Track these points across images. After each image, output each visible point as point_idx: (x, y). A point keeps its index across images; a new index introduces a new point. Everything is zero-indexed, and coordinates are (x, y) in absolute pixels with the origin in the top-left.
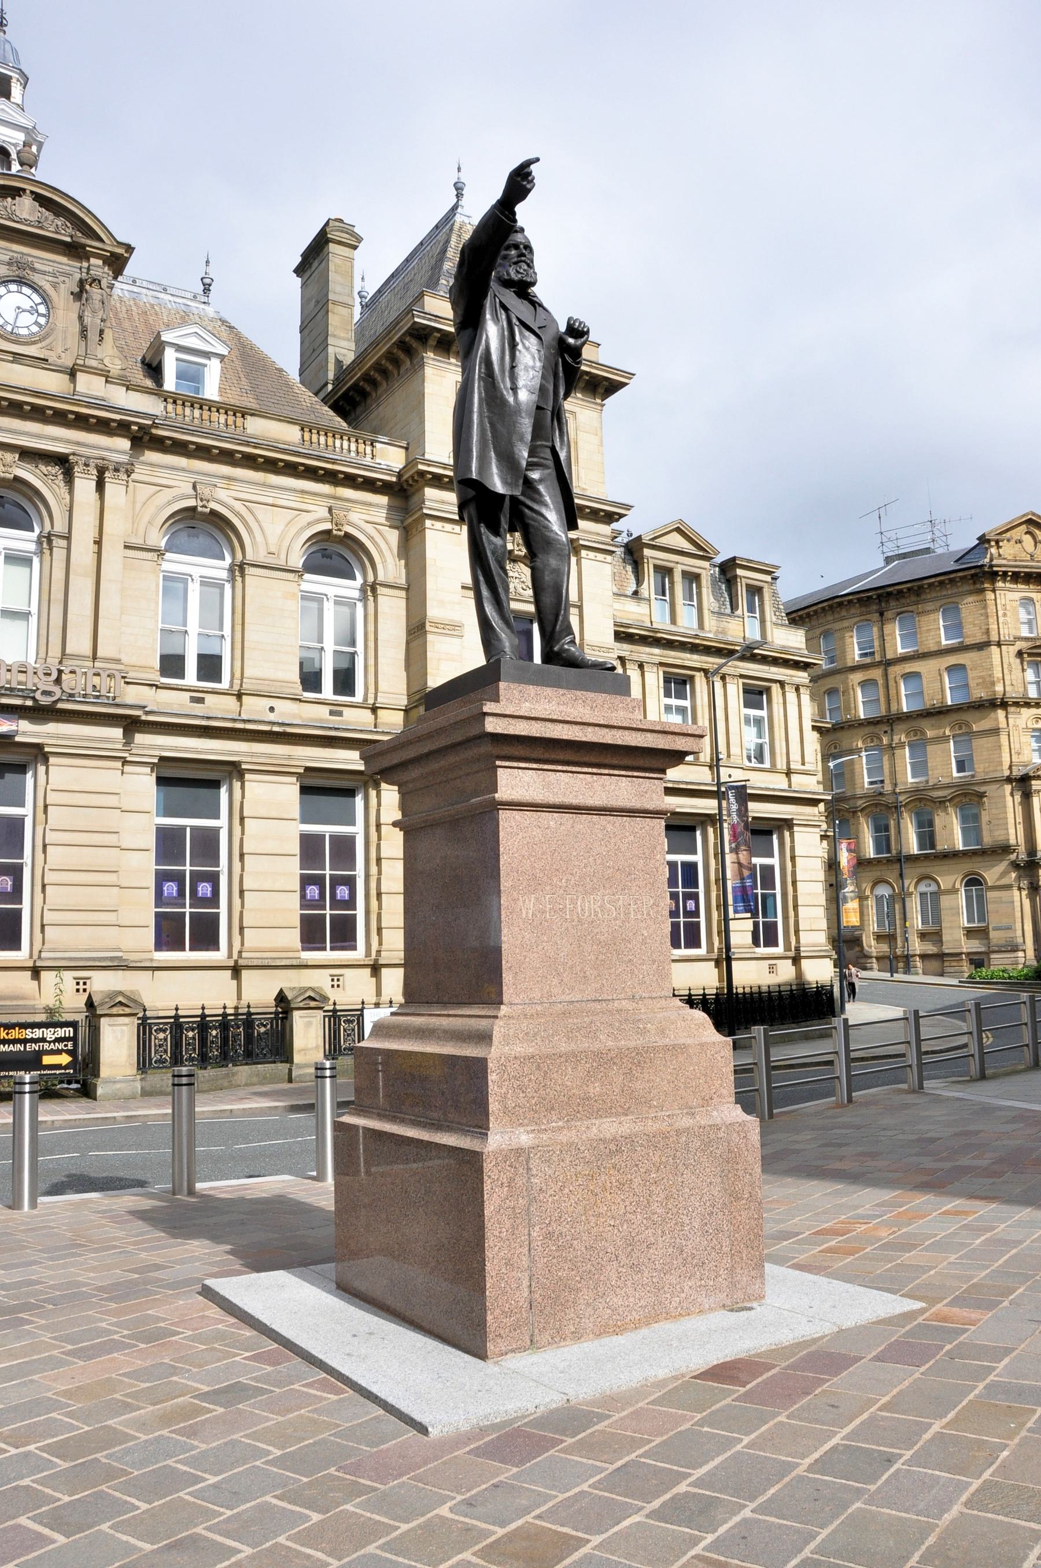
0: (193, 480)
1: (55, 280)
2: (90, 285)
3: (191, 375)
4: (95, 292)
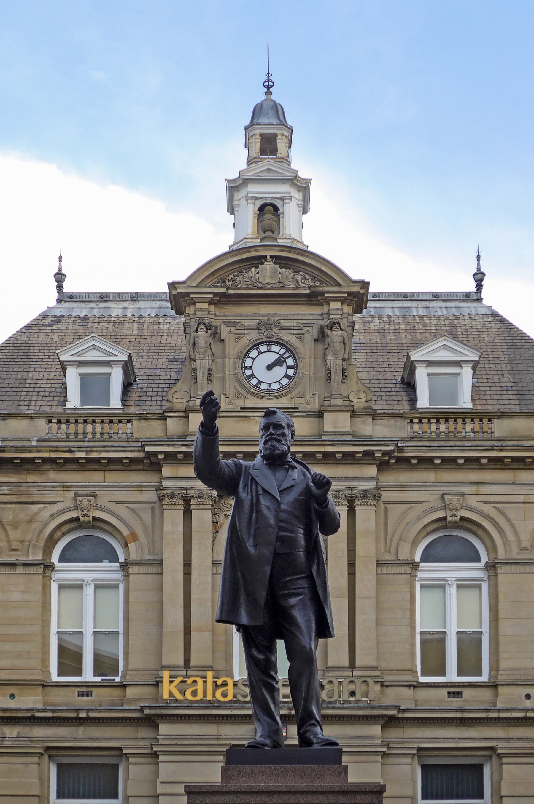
0: (441, 493)
1: (300, 332)
2: (331, 329)
3: (443, 385)
4: (336, 335)
